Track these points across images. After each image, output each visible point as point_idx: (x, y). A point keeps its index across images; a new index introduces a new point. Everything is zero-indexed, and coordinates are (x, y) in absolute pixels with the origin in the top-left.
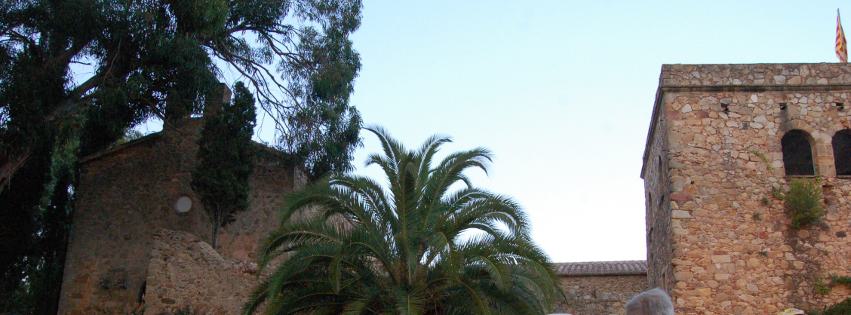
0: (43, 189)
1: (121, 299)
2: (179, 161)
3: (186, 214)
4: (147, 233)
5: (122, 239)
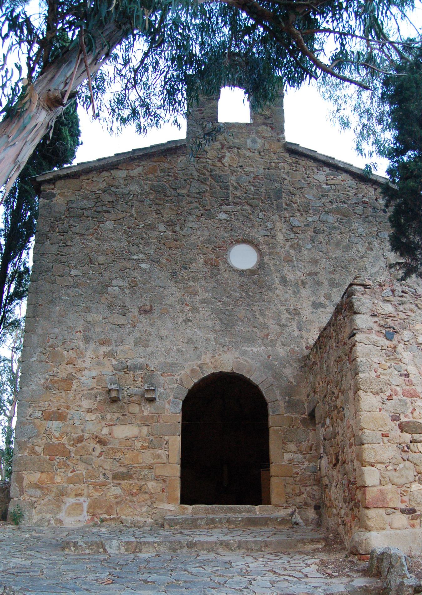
0: (397, 128)
1: (146, 422)
2: (227, 188)
3: (252, 272)
4: (182, 302)
5: (135, 312)
